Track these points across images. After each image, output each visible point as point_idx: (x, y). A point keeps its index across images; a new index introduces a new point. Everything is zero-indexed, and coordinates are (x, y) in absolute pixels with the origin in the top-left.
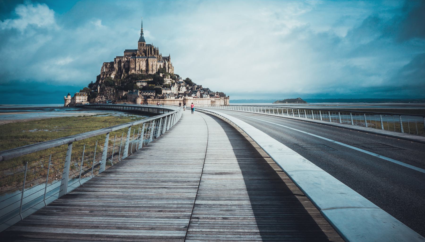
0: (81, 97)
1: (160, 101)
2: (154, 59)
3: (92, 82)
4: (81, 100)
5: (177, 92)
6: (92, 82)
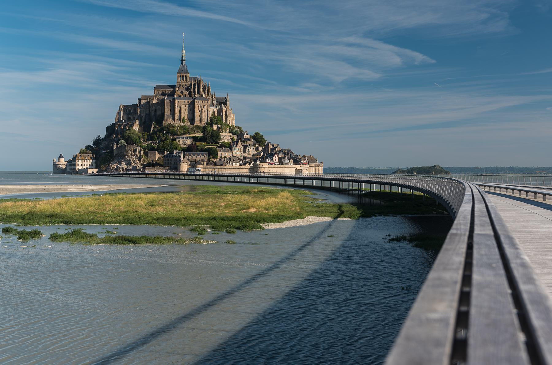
0: (86, 161)
1: (216, 168)
2: (204, 101)
3: (99, 136)
4: (86, 165)
5: (242, 155)
6: (99, 136)
